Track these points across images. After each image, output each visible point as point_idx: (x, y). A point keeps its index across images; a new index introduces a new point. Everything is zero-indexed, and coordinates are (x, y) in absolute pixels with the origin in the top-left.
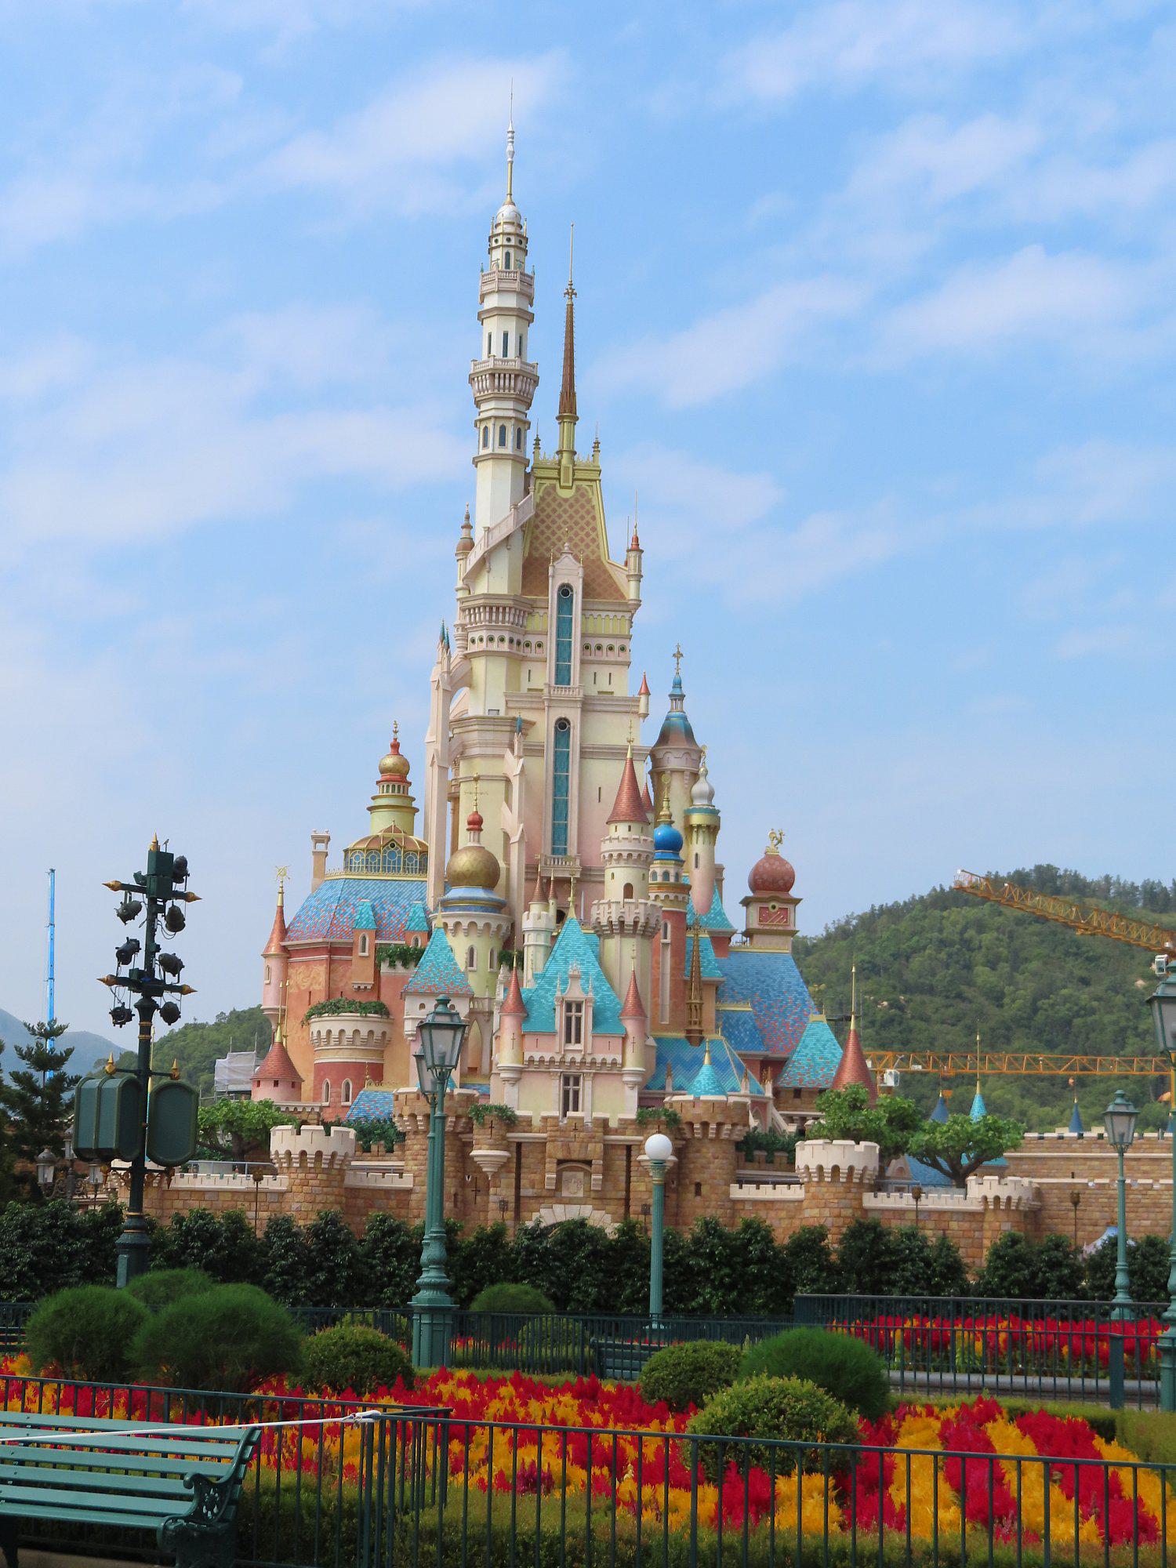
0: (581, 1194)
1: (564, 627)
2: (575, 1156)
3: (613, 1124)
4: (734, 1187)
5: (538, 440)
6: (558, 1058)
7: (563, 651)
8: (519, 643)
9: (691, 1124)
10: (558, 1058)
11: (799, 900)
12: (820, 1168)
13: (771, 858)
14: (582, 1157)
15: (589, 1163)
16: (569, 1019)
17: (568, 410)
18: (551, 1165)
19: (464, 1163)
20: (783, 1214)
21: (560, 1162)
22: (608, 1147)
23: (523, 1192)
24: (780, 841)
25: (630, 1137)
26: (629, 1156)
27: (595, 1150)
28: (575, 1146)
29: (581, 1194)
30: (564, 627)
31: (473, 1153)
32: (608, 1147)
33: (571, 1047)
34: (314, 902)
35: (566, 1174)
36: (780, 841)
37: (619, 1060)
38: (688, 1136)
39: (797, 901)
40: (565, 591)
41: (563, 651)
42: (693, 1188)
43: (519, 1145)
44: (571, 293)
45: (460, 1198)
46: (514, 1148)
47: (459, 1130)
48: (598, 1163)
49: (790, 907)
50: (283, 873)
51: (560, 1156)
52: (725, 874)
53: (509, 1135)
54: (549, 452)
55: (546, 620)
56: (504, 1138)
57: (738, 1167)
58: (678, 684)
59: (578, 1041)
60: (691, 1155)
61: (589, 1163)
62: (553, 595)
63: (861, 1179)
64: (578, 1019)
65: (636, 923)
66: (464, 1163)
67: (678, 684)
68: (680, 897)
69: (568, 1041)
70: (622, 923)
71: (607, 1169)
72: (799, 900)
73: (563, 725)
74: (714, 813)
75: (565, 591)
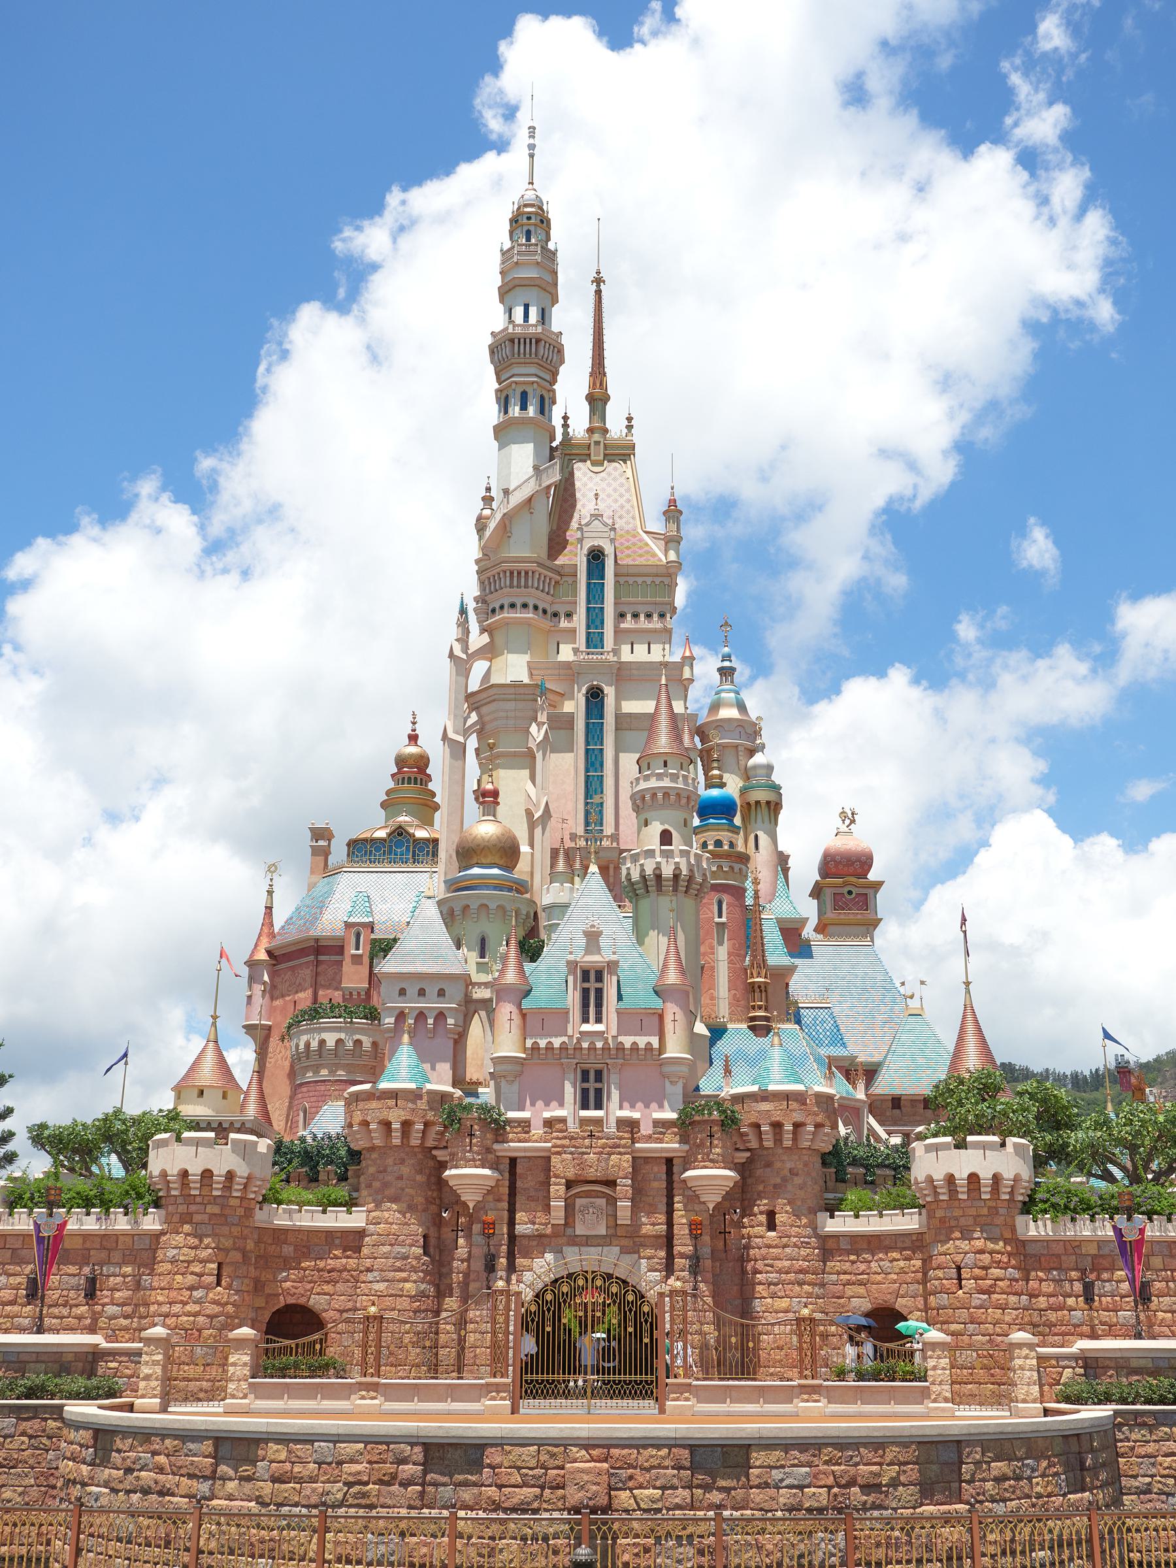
0: (603, 1231)
2: (592, 1173)
4: (823, 1216)
5: (565, 418)
7: (595, 618)
8: (545, 612)
11: (880, 884)
14: (599, 1175)
15: (612, 1184)
17: (597, 400)
18: (557, 1189)
19: (440, 1190)
22: (639, 1162)
23: (520, 1229)
24: (853, 821)
26: (670, 1173)
27: (621, 1163)
31: (447, 1173)
32: (639, 1162)
33: (586, 1027)
34: (308, 902)
35: (579, 1202)
36: (853, 821)
37: (656, 1045)
39: (877, 885)
41: (595, 618)
43: (513, 1161)
44: (598, 281)
45: (433, 1241)
47: (430, 1143)
48: (625, 1186)
49: (870, 892)
51: (571, 1173)
52: (791, 863)
53: (496, 1146)
56: (489, 1150)
57: (827, 1190)
60: (759, 1172)
61: (612, 1184)
63: (1012, 1193)
64: (599, 992)
65: (676, 877)
66: (440, 1190)
68: (737, 866)
70: (658, 877)
72: (880, 884)
74: (776, 788)
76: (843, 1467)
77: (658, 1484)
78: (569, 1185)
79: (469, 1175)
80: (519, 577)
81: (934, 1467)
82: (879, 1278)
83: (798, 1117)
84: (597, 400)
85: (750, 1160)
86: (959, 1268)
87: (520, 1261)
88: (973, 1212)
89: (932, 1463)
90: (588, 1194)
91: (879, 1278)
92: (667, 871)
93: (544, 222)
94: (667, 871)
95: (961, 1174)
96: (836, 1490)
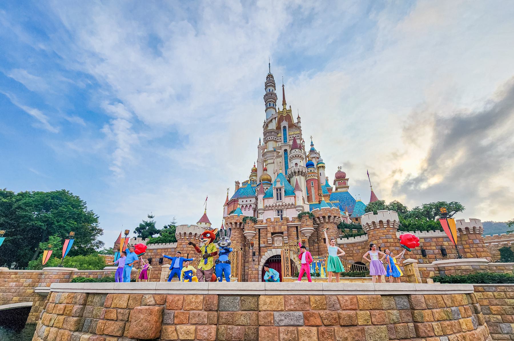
0: (281, 245)
1: (285, 134)
2: (277, 231)
3: (291, 219)
6: (274, 205)
9: (319, 218)
10: (274, 205)
12: (374, 223)
13: (339, 171)
14: (280, 231)
16: (277, 194)
17: (284, 103)
18: (269, 235)
20: (360, 248)
21: (273, 234)
25: (297, 223)
27: (284, 228)
28: (277, 227)
29: (281, 245)
30: (285, 134)
35: (275, 238)
38: (319, 222)
39: (347, 180)
40: (285, 127)
42: (323, 240)
44: (283, 86)
46: (257, 231)
48: (285, 233)
50: (228, 189)
51: (272, 231)
54: (281, 110)
55: (281, 134)
58: (312, 142)
59: (281, 199)
61: (282, 233)
62: (282, 128)
64: (280, 193)
65: (299, 172)
67: (312, 142)
69: (278, 200)
70: (295, 172)
71: (289, 235)
73: (286, 150)
75: (285, 127)
76: (328, 312)
77: (193, 321)
78: (273, 234)
79: (249, 232)
80: (271, 132)
81: (395, 312)
82: (356, 255)
83: (329, 214)
84: (284, 103)
85: (318, 227)
86: (380, 248)
87: (262, 253)
88: (382, 231)
89: (393, 309)
90: (278, 236)
91: (356, 255)
92: (297, 171)
93: (272, 77)
94: (297, 171)
95: (377, 221)
96: (323, 328)
